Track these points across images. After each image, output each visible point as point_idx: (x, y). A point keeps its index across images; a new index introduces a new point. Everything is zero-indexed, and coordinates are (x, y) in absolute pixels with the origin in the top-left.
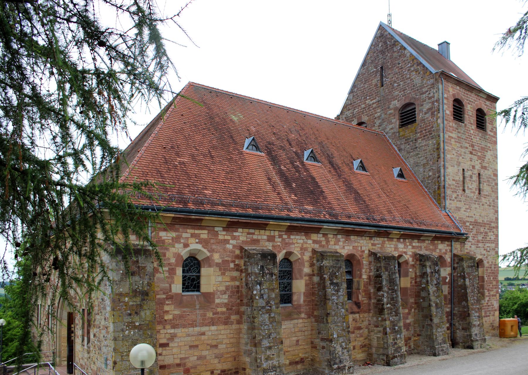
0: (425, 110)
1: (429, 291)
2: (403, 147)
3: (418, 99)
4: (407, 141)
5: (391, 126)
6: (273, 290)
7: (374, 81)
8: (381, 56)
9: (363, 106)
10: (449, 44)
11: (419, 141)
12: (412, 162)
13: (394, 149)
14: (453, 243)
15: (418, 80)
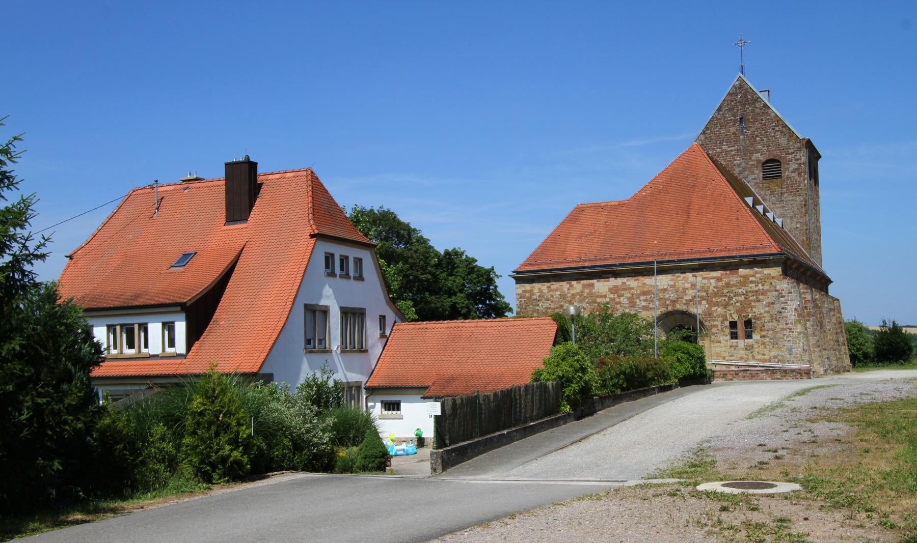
0: (791, 169)
2: (767, 197)
3: (783, 158)
4: (772, 193)
5: (753, 176)
6: (632, 304)
7: (733, 130)
8: (740, 107)
11: (786, 195)
15: (783, 141)
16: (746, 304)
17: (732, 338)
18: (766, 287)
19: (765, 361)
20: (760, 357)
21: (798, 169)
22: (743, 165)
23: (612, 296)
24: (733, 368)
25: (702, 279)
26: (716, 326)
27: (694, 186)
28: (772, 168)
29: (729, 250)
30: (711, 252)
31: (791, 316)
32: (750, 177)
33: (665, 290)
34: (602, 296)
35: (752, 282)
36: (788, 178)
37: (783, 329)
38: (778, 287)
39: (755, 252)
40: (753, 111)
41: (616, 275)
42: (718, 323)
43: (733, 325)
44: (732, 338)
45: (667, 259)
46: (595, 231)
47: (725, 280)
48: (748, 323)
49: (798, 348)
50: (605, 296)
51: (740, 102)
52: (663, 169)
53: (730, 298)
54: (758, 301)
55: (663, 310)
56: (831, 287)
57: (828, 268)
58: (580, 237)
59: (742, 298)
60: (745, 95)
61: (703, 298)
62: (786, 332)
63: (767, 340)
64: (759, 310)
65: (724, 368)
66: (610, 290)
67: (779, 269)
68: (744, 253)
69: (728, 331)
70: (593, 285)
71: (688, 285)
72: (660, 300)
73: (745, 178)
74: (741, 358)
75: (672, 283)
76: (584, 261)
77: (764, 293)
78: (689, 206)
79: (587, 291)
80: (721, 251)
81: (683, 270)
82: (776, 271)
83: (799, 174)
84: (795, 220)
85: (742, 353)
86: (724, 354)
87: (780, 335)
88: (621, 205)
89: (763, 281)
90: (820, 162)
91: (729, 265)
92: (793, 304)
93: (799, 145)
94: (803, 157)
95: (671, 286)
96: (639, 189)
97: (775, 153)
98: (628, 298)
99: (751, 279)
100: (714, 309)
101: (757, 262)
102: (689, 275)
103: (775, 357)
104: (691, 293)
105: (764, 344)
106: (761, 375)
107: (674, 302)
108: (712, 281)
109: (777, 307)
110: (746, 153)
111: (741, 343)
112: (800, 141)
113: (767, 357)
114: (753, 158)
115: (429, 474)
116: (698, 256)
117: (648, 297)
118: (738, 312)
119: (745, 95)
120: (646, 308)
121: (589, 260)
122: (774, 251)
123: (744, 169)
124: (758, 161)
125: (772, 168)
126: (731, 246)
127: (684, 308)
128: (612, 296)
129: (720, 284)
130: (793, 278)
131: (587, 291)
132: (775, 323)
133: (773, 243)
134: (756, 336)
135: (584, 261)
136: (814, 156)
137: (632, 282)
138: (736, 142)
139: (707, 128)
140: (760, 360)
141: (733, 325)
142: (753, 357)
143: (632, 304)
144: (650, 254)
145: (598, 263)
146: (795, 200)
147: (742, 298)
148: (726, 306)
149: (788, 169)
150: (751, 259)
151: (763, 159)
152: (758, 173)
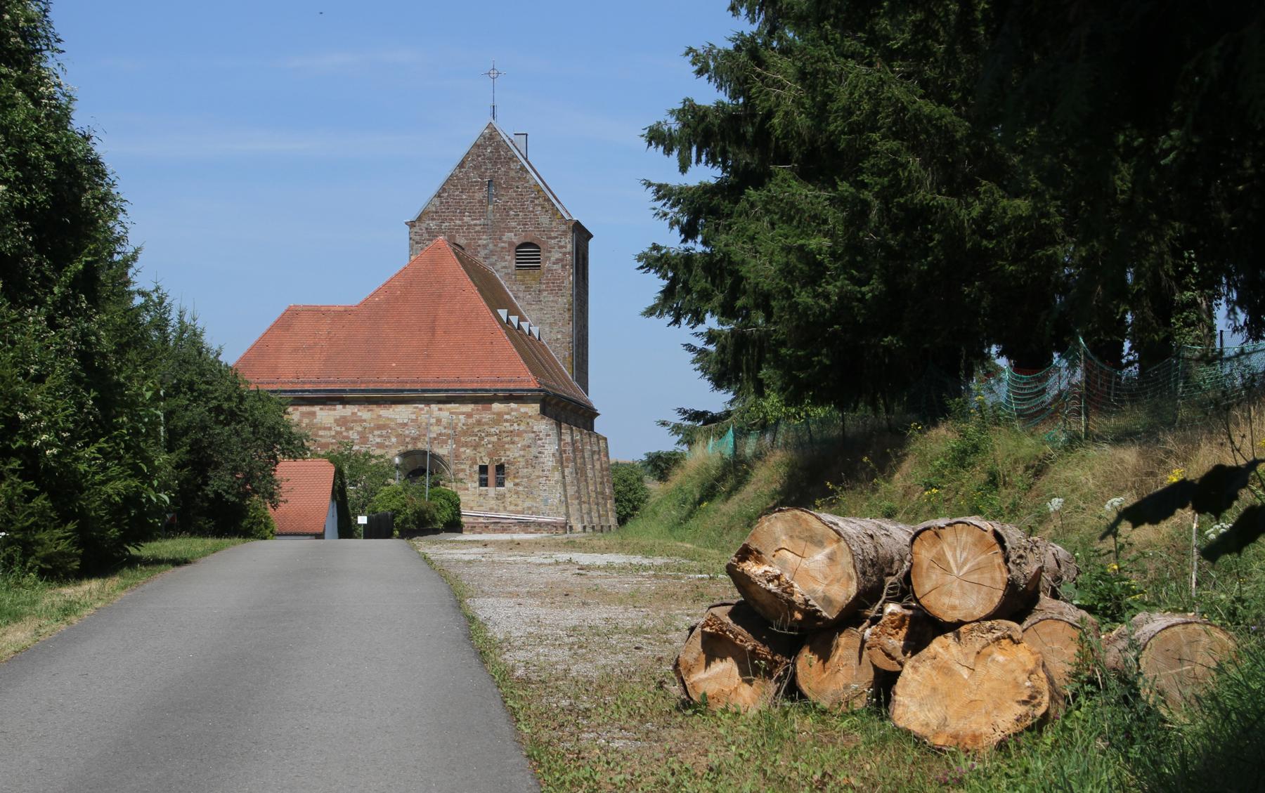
0: (553, 259)
1: (458, 561)
2: (521, 295)
3: (544, 243)
4: (528, 289)
5: (504, 264)
6: (364, 439)
7: (479, 196)
8: (489, 166)
9: (458, 222)
10: (590, 236)
11: (545, 294)
12: (534, 316)
13: (560, 369)
14: (132, 288)
15: (544, 220)
16: (499, 446)
17: (481, 485)
18: (522, 428)
19: (518, 512)
20: (512, 508)
21: (562, 260)
22: (491, 246)
23: (338, 429)
24: (481, 520)
25: (444, 413)
26: (463, 470)
27: (440, 296)
28: (528, 254)
29: (482, 382)
30: (461, 382)
31: (548, 461)
32: (499, 266)
33: (406, 424)
34: (325, 429)
35: (507, 421)
36: (549, 270)
37: (539, 477)
38: (535, 429)
39: (512, 387)
40: (506, 173)
41: (344, 402)
42: (466, 467)
43: (483, 469)
44: (481, 485)
45: (408, 387)
46: (315, 344)
47: (477, 416)
48: (500, 468)
49: (556, 497)
50: (330, 429)
51: (489, 159)
52: (401, 268)
53: (481, 439)
54: (513, 443)
55: (402, 448)
56: (597, 422)
57: (596, 396)
58: (296, 350)
59: (494, 439)
60: (497, 149)
61: (449, 436)
62: (543, 480)
63: (521, 488)
64: (513, 453)
65: (471, 520)
66: (336, 420)
67: (537, 406)
68: (499, 386)
69: (477, 477)
70: (314, 414)
71: (433, 421)
72: (398, 436)
73: (493, 265)
74: (491, 509)
75: (414, 417)
76: (304, 383)
77: (519, 434)
78: (434, 321)
79: (306, 421)
80: (472, 382)
81: (428, 401)
82: (534, 409)
83: (564, 266)
84: (556, 329)
85: (493, 503)
86: (472, 504)
87: (535, 483)
88: (347, 311)
89: (519, 420)
90: (591, 242)
91: (482, 399)
92: (551, 448)
93: (564, 227)
94: (568, 244)
95: (412, 420)
96: (371, 292)
97: (533, 235)
98: (358, 433)
99: (506, 417)
100: (462, 450)
101: (511, 397)
102: (434, 407)
103: (529, 508)
104: (435, 430)
105: (517, 493)
106: (514, 528)
107: (415, 440)
108: (462, 417)
109: (534, 451)
110: (495, 230)
111: (492, 491)
112: (566, 222)
113: (519, 508)
114: (504, 238)
115: (924, 553)
116: (445, 386)
117: (384, 432)
118: (490, 455)
119: (497, 149)
120: (379, 446)
121: (310, 382)
122: (533, 386)
123: (492, 253)
124: (511, 244)
125: (528, 254)
126: (483, 378)
127: (426, 447)
128: (338, 429)
129: (470, 421)
130: (551, 417)
131: (306, 421)
132: (530, 470)
133: (532, 377)
134: (509, 484)
135: (304, 383)
136: (582, 235)
137: (364, 413)
138: (483, 214)
139: (443, 189)
140: (512, 512)
141: (483, 469)
142: (505, 508)
143: (364, 439)
144: (387, 381)
145: (322, 387)
146: (556, 302)
147: (494, 439)
148: (475, 447)
149: (548, 258)
150: (507, 394)
151: (517, 241)
152: (510, 260)
